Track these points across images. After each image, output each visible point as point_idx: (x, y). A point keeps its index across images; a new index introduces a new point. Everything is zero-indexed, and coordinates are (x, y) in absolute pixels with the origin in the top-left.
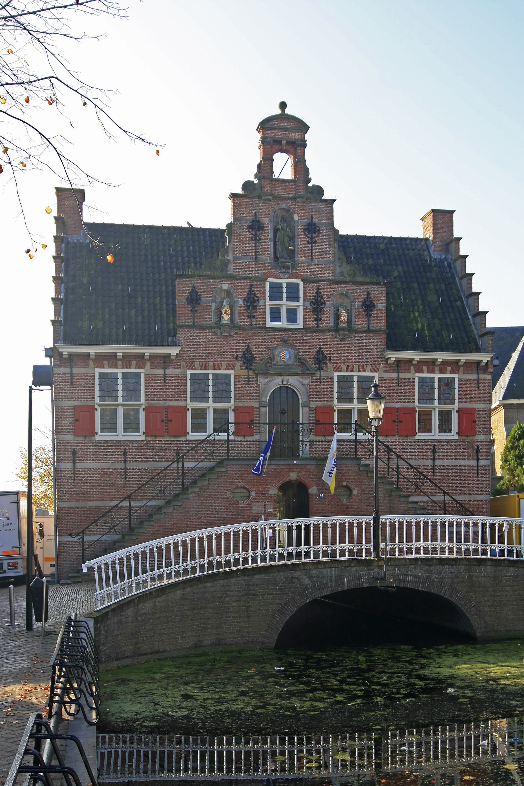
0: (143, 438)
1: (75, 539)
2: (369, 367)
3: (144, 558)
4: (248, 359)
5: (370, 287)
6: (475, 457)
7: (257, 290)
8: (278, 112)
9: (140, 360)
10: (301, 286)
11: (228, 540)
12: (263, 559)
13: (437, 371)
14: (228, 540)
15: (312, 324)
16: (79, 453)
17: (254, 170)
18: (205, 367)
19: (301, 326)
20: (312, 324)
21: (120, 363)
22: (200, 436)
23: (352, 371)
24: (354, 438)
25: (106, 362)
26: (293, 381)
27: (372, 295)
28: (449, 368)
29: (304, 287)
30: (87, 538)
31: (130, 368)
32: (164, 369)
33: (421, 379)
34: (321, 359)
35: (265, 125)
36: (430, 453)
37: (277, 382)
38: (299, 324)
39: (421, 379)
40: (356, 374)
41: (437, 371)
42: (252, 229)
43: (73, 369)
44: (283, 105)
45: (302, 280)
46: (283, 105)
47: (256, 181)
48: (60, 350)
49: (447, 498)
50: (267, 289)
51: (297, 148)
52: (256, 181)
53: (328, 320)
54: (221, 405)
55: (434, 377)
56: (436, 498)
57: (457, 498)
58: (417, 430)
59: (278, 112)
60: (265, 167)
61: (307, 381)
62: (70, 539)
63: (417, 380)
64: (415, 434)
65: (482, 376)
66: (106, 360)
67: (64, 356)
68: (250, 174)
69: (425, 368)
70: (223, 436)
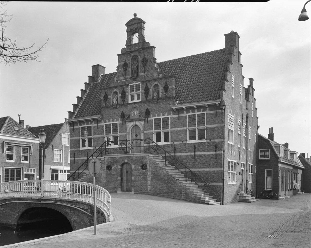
4: (123, 116)
5: (106, 90)
6: (215, 150)
7: (125, 89)
8: (134, 17)
9: (204, 108)
10: (141, 84)
13: (196, 112)
18: (159, 115)
21: (196, 110)
23: (160, 116)
24: (148, 145)
25: (191, 111)
26: (137, 123)
27: (167, 82)
28: (202, 109)
29: (142, 85)
31: (88, 124)
32: (98, 123)
33: (189, 116)
34: (148, 113)
36: (193, 149)
39: (189, 116)
40: (111, 123)
41: (196, 112)
42: (144, 62)
43: (179, 115)
44: (135, 15)
45: (141, 82)
47: (126, 47)
48: (172, 108)
49: (188, 170)
53: (151, 96)
54: (201, 127)
55: (195, 114)
59: (134, 17)
60: (129, 40)
61: (143, 122)
63: (187, 117)
67: (217, 105)
69: (191, 111)
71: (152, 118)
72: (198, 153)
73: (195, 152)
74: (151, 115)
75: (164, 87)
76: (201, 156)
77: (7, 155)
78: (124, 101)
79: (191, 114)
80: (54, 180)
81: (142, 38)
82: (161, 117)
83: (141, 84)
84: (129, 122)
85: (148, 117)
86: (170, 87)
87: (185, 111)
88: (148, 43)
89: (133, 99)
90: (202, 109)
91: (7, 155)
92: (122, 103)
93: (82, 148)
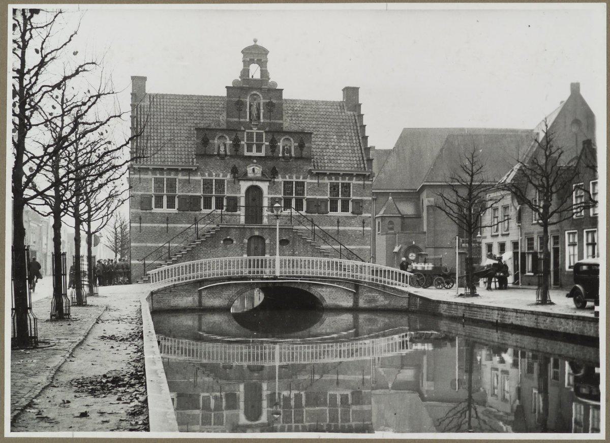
0: (177, 212)
1: (141, 262)
2: (301, 177)
3: (165, 272)
4: (234, 171)
11: (190, 268)
12: (254, 273)
14: (190, 268)
15: (270, 154)
16: (143, 218)
17: (239, 74)
19: (264, 155)
20: (270, 154)
22: (208, 211)
30: (146, 262)
35: (246, 52)
37: (249, 184)
38: (263, 154)
44: (255, 41)
46: (255, 41)
47: (240, 80)
49: (342, 247)
50: (245, 136)
51: (262, 63)
52: (240, 80)
56: (336, 247)
57: (347, 247)
58: (329, 210)
59: (253, 43)
60: (245, 72)
62: (137, 262)
64: (328, 213)
65: (366, 182)
66: (413, 252)
68: (237, 76)
70: (219, 211)
71: (279, 179)
72: (341, 228)
73: (167, 227)
74: (280, 175)
75: (203, 140)
76: (344, 231)
77: (342, 211)
78: (237, 150)
79: (334, 181)
80: (559, 246)
81: (264, 73)
82: (294, 180)
83: (264, 134)
84: (244, 180)
85: (274, 178)
86: (306, 145)
87: (354, 178)
88: (234, 82)
89: (250, 150)
90: (347, 178)
91: (342, 211)
92: (234, 153)
93: (155, 210)
